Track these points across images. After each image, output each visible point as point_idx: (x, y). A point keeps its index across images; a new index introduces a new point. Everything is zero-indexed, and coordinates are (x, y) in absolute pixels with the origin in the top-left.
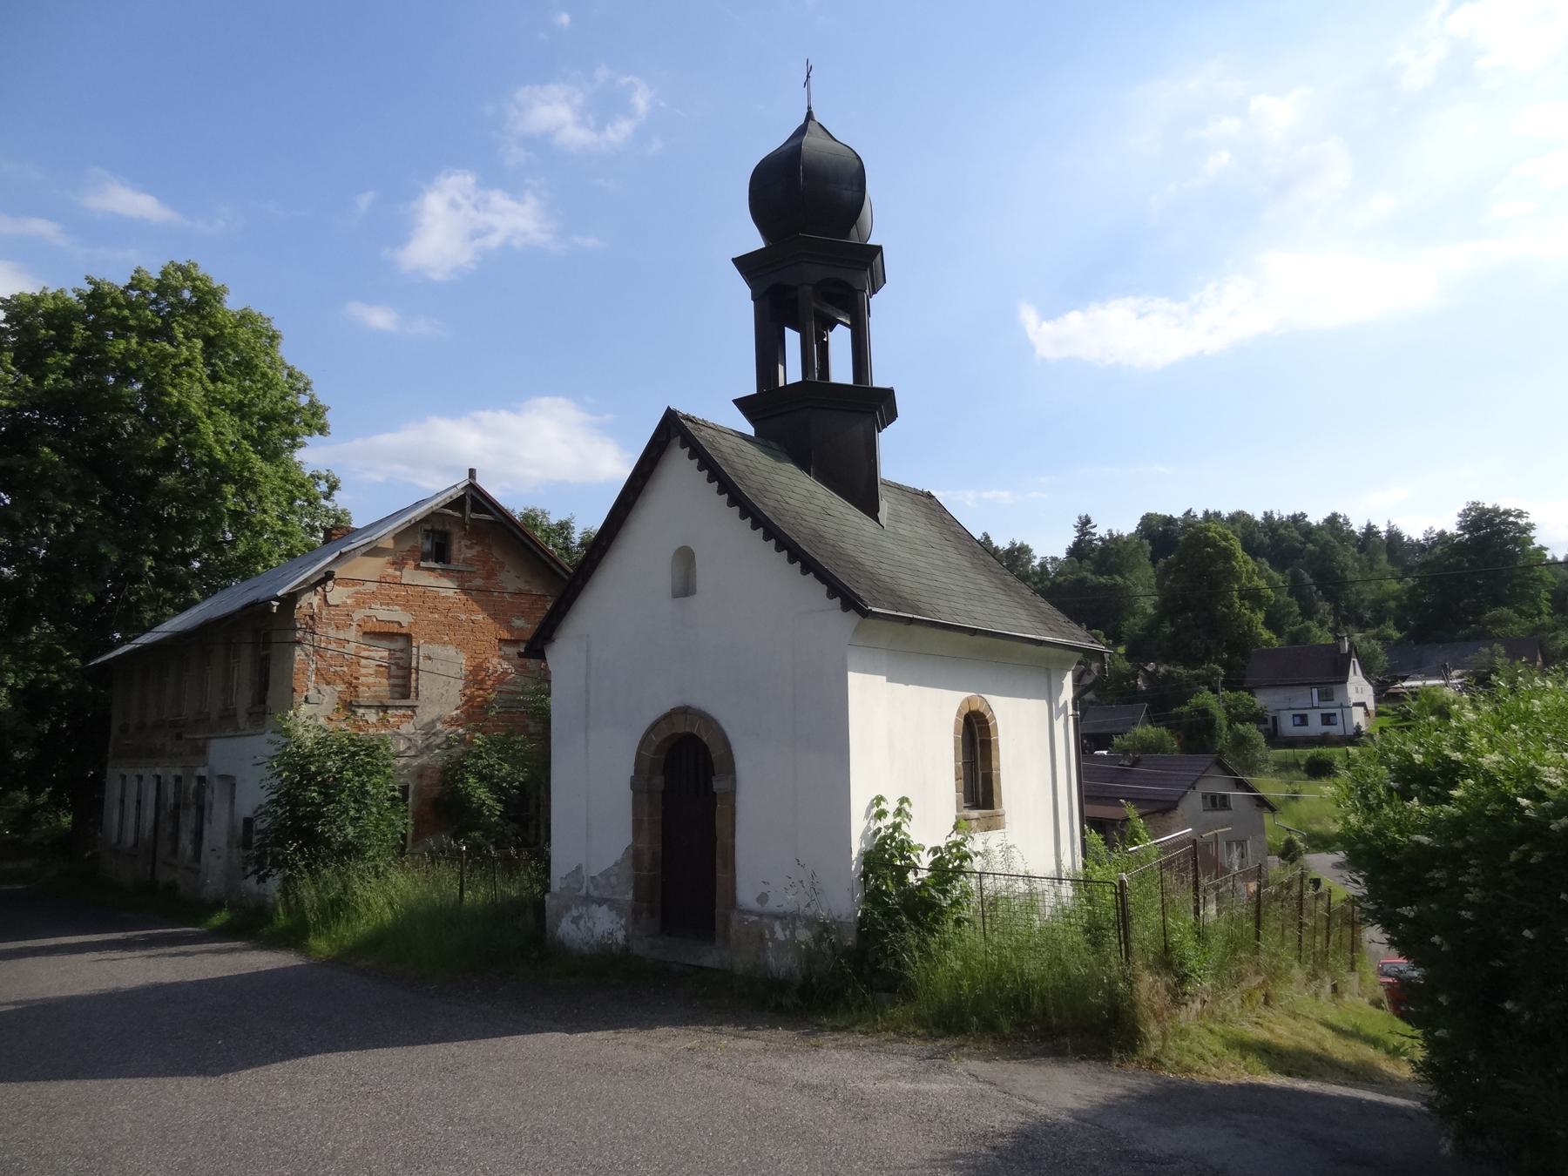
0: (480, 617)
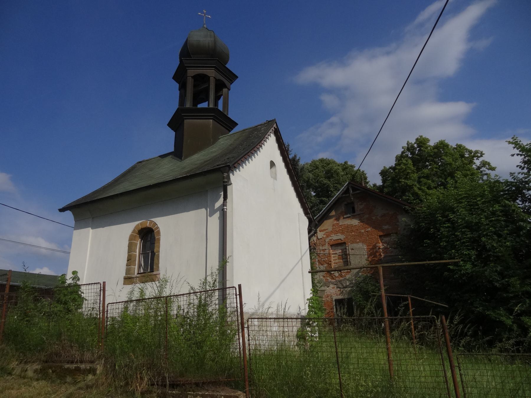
0: (369, 229)
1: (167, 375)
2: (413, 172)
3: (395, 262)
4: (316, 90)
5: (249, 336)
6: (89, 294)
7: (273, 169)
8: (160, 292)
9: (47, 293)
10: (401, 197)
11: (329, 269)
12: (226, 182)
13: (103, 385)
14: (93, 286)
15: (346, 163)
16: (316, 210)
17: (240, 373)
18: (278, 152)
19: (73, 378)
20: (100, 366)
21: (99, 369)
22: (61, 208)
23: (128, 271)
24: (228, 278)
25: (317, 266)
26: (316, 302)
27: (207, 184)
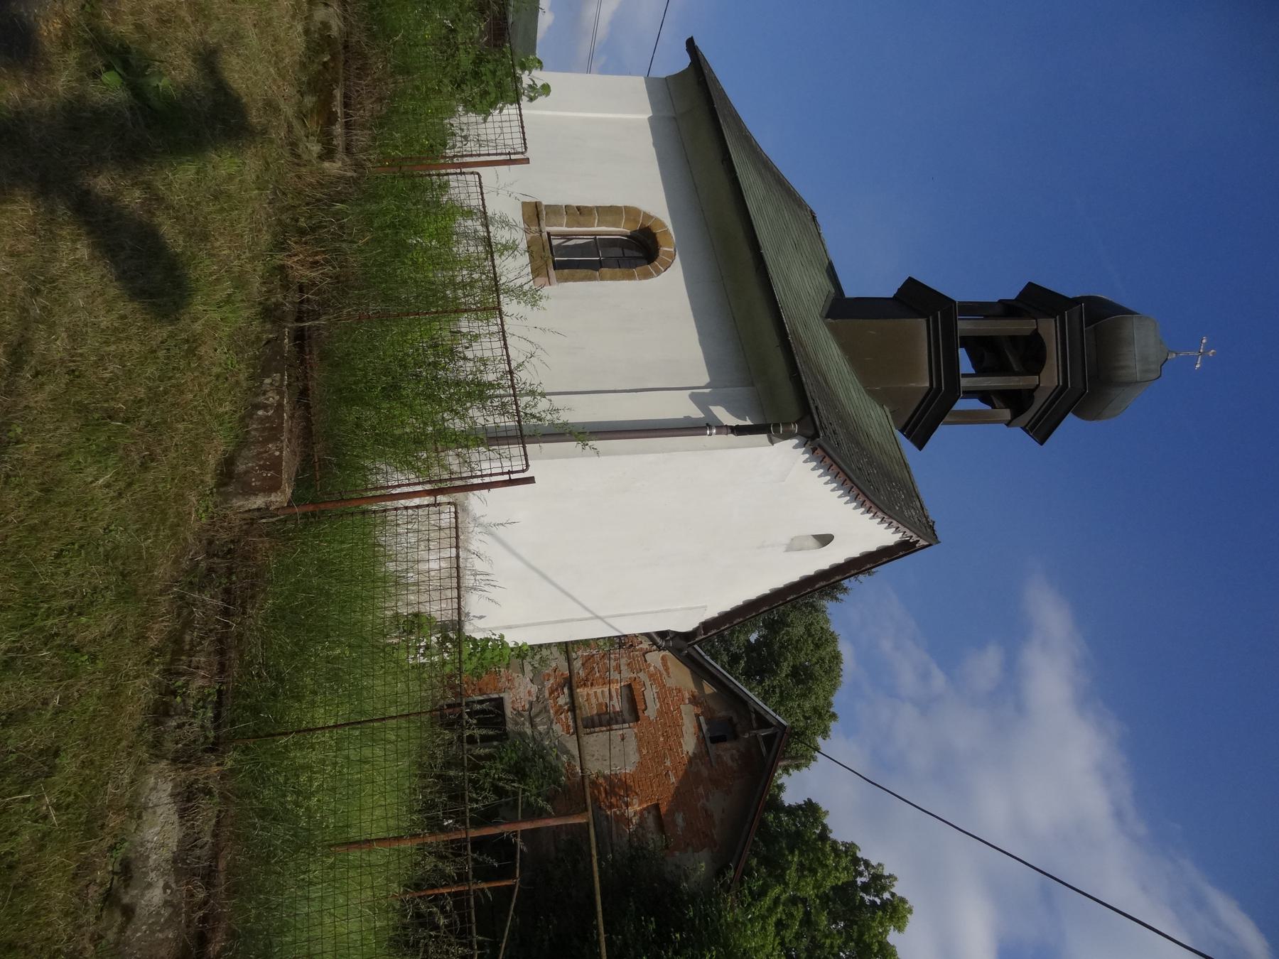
0: (673, 780)
1: (322, 321)
2: (817, 886)
3: (599, 853)
4: (1013, 632)
5: (418, 507)
6: (499, 126)
7: (813, 542)
8: (509, 291)
9: (499, 32)
10: (756, 854)
11: (575, 680)
12: (777, 431)
13: (299, 177)
14: (520, 135)
15: (834, 716)
16: (713, 646)
17: (330, 490)
18: (855, 552)
19: (312, 111)
20: (339, 169)
21: (333, 167)
22: (697, 43)
23: (554, 210)
24: (547, 447)
25: (580, 653)
26: (495, 655)
27: (770, 384)
